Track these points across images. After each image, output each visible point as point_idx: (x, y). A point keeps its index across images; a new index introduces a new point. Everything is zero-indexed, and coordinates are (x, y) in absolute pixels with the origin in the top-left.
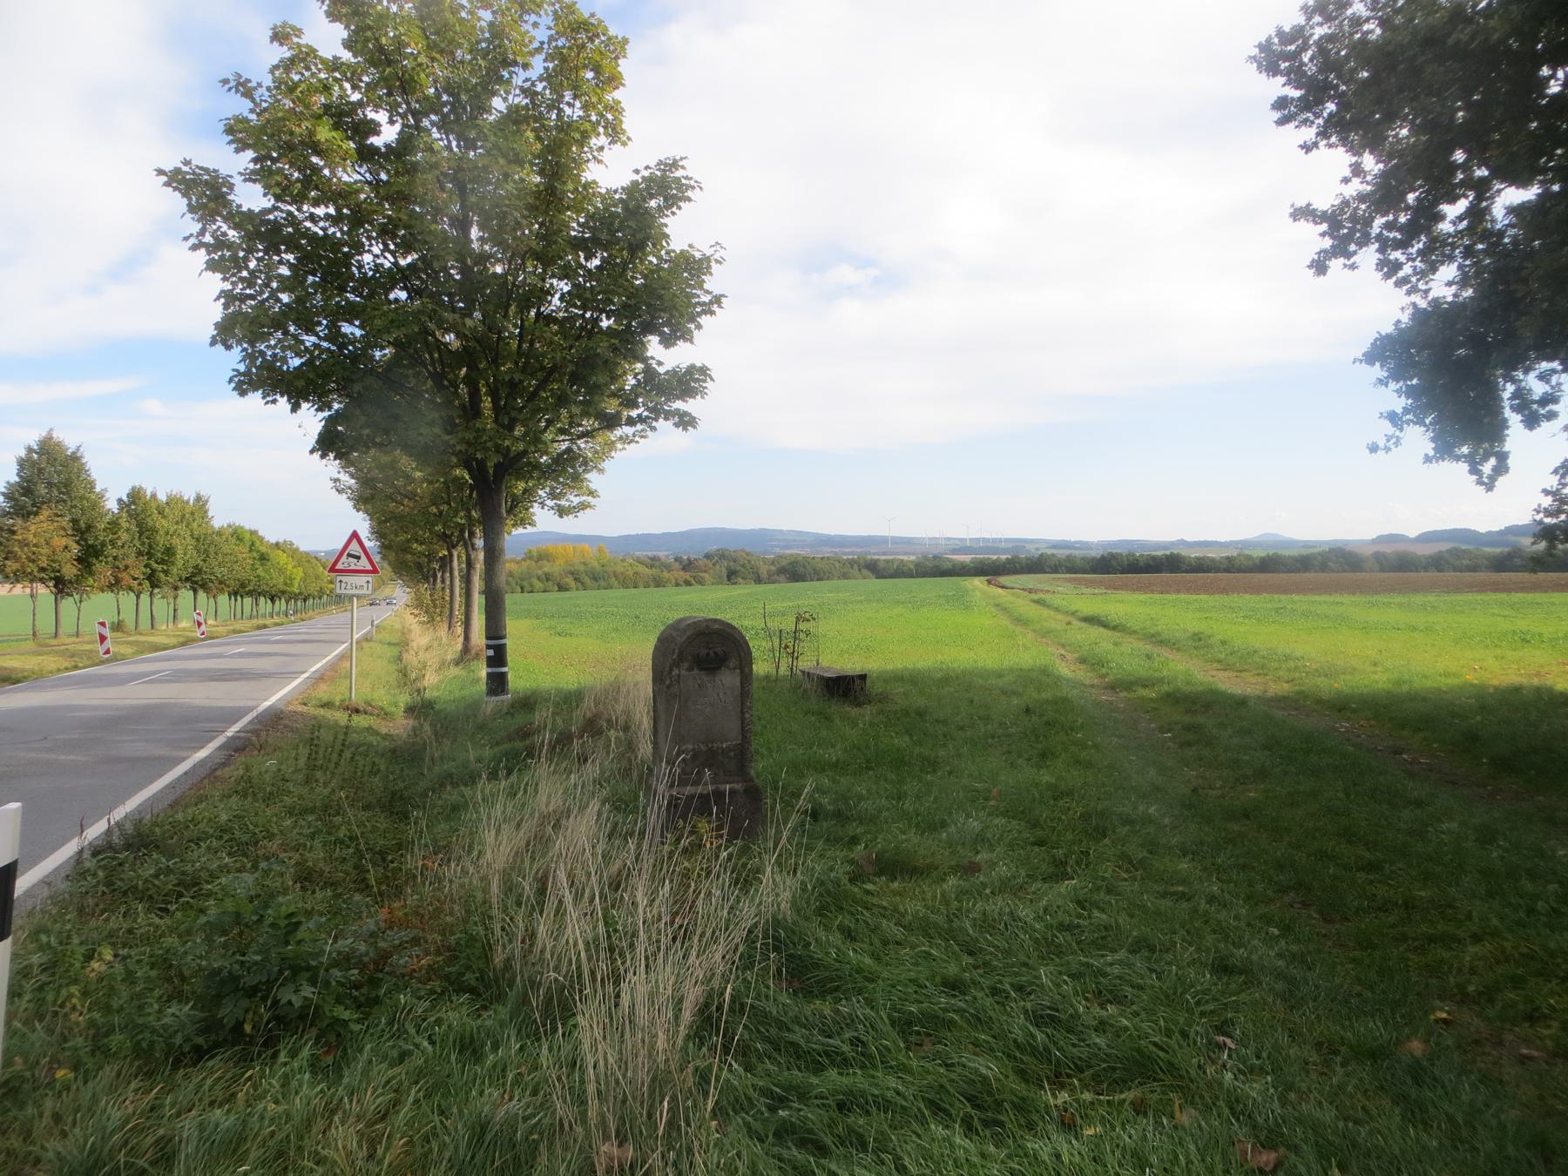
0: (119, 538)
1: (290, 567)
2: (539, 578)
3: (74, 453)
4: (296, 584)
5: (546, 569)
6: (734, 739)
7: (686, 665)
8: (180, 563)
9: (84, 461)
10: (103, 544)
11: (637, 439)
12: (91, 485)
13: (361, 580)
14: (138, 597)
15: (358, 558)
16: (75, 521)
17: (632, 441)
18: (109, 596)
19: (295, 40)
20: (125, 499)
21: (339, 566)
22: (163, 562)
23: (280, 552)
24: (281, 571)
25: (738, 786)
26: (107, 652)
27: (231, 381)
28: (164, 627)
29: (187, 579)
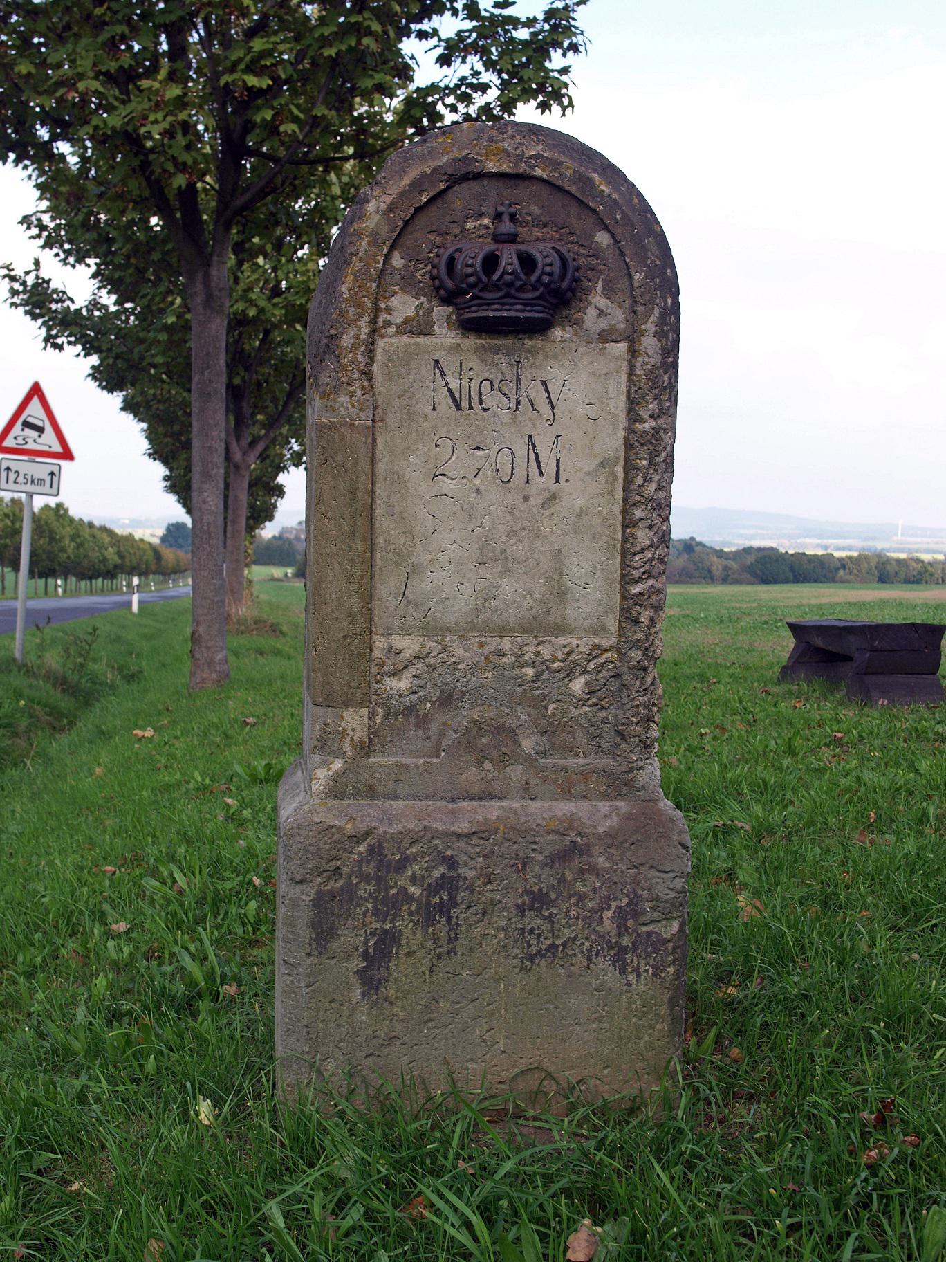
15: (40, 430)
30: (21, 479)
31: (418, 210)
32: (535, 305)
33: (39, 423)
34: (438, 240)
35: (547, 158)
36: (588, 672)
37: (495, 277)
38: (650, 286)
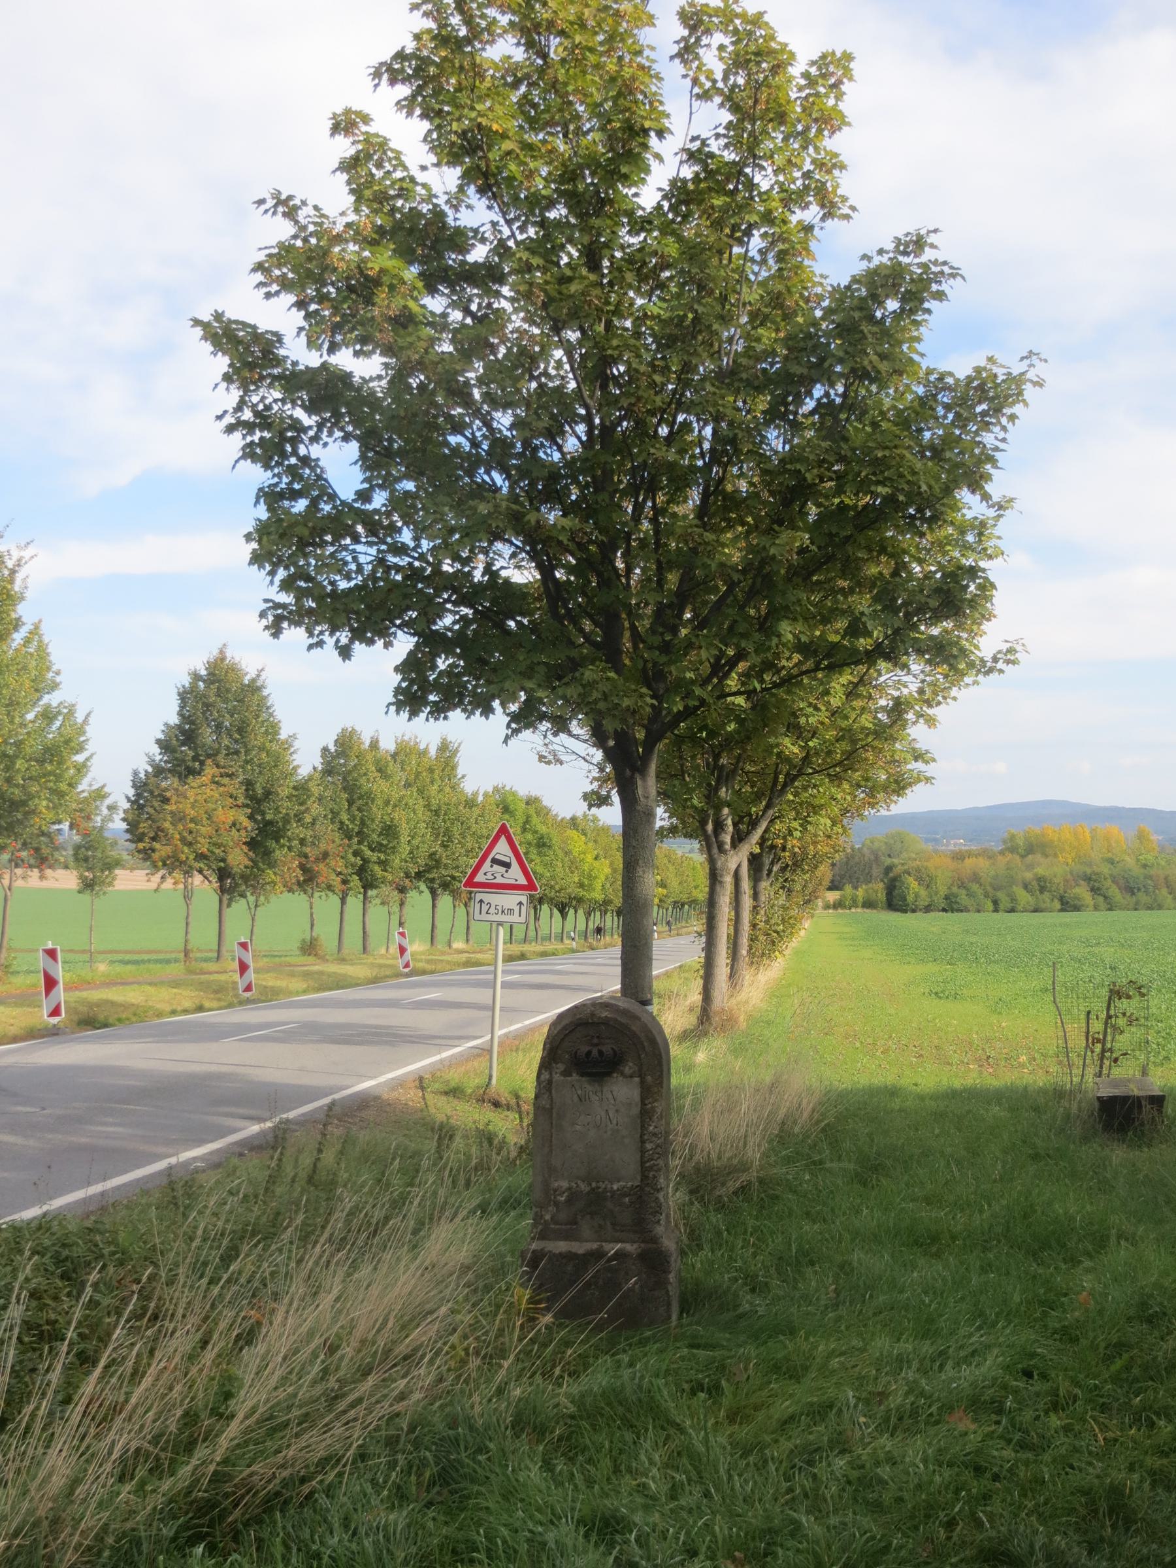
0: (307, 810)
1: (589, 858)
2: (1026, 887)
3: (253, 681)
4: (598, 885)
5: (1040, 871)
6: (629, 1178)
7: (561, 1067)
8: (405, 849)
9: (265, 692)
10: (286, 820)
11: (1000, 665)
12: (273, 729)
13: (510, 900)
14: (343, 901)
15: (507, 865)
16: (249, 784)
17: (990, 671)
18: (299, 900)
19: (364, 128)
20: (332, 749)
21: (479, 878)
22: (380, 848)
23: (574, 834)
24: (574, 865)
25: (630, 1248)
26: (248, 988)
27: (263, 615)
28: (383, 951)
29: (419, 875)
30: (492, 910)
33: (507, 860)
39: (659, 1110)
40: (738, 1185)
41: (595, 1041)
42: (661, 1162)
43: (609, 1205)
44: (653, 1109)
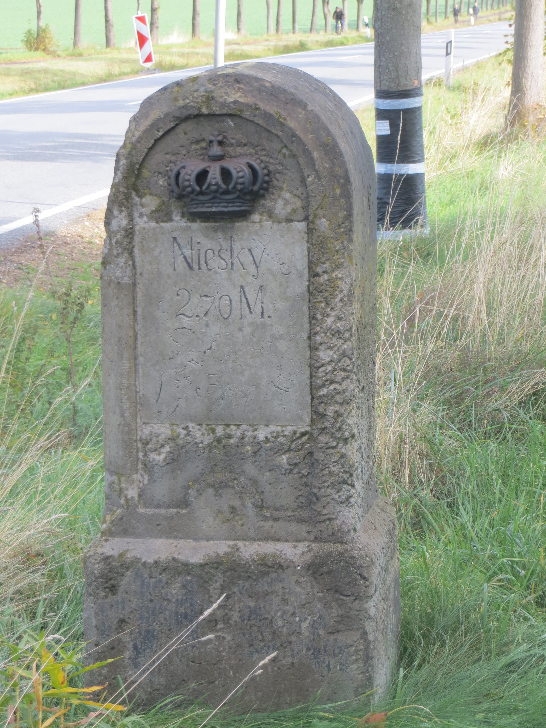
31: (157, 141)
32: (234, 203)
34: (173, 158)
35: (242, 103)
36: (292, 450)
37: (204, 187)
38: (318, 185)
39: (344, 286)
40: (528, 389)
41: (216, 150)
42: (351, 386)
43: (250, 469)
44: (333, 283)
